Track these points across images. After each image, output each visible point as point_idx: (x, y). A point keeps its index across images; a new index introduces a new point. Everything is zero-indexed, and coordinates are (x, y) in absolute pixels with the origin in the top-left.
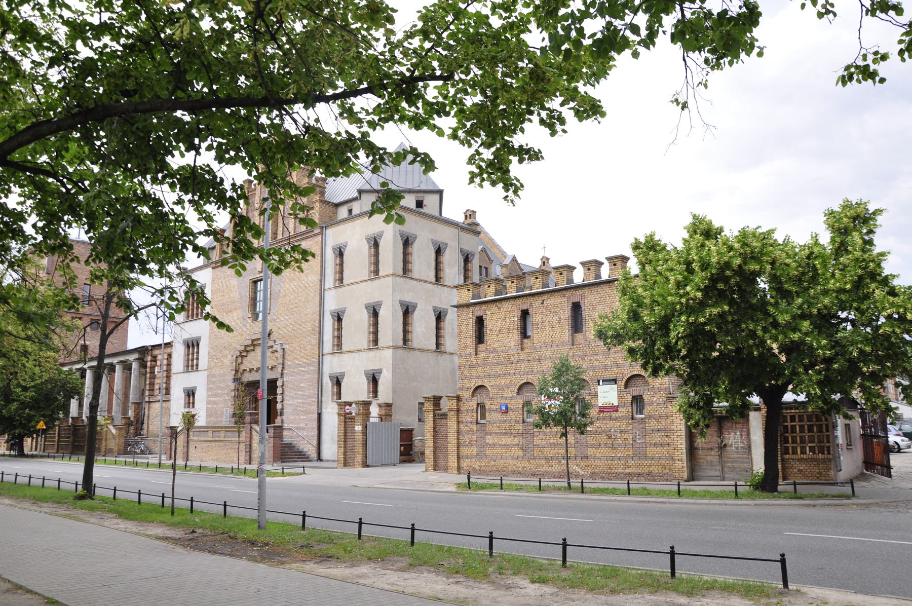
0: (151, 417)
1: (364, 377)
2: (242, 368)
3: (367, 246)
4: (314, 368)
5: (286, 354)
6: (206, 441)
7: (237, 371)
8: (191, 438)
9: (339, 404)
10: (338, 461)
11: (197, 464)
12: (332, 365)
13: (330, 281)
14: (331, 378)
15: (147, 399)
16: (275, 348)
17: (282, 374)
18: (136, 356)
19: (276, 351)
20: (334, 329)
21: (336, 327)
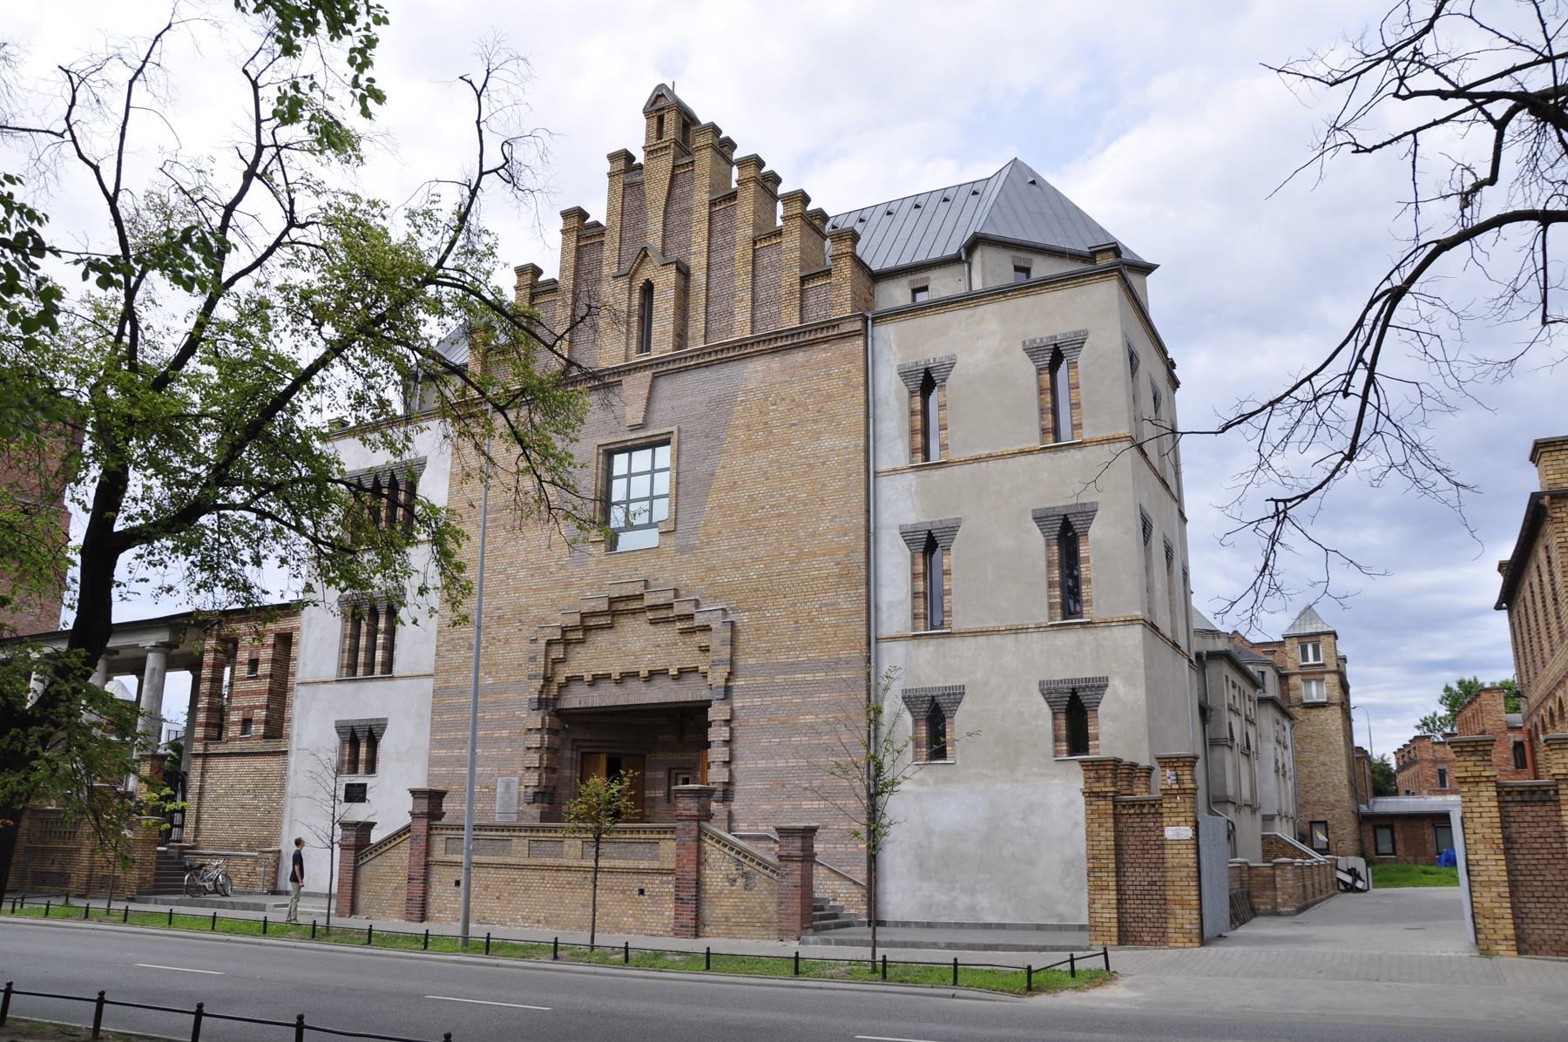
0: (208, 797)
1: (1041, 699)
2: (563, 673)
3: (1032, 369)
4: (855, 673)
5: (742, 637)
6: (507, 866)
7: (548, 680)
8: (438, 853)
9: (1088, 766)
10: (1090, 928)
11: (618, 940)
12: (911, 665)
13: (894, 447)
14: (910, 700)
15: (198, 748)
16: (699, 620)
17: (728, 691)
18: (164, 637)
19: (706, 629)
20: (914, 576)
21: (920, 568)
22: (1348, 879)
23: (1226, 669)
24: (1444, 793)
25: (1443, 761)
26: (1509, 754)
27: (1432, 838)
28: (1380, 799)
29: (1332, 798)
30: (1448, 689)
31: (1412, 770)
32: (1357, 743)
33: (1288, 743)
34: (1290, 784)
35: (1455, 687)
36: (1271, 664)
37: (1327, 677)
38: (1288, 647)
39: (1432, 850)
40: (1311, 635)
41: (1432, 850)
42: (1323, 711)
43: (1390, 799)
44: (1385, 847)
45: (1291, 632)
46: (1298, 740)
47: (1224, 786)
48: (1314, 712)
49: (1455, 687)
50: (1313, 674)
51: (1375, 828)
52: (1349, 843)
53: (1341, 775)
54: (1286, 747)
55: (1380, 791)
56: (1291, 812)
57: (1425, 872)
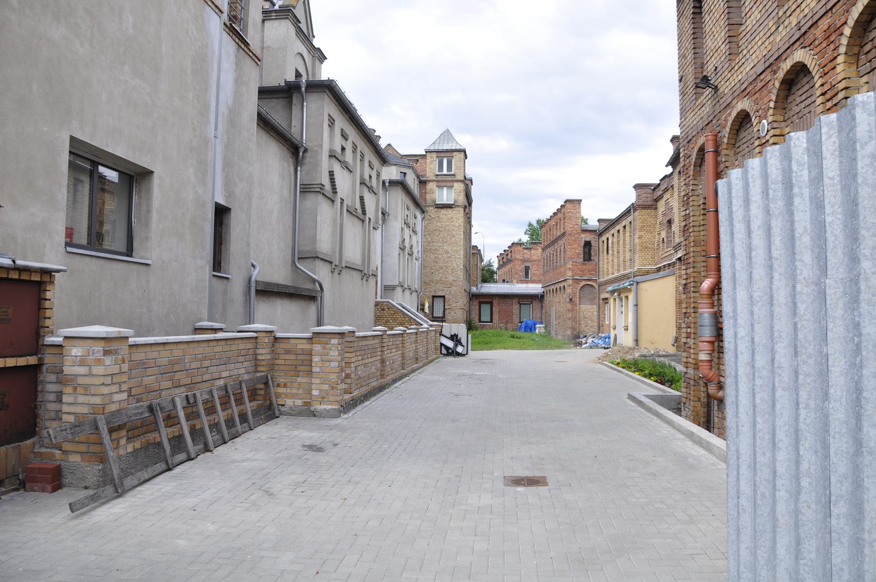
22: (450, 344)
23: (329, 108)
24: (527, 282)
25: (528, 261)
26: (580, 250)
27: (517, 312)
28: (485, 285)
29: (451, 278)
30: (530, 225)
31: (508, 267)
32: (473, 243)
33: (419, 229)
34: (417, 264)
35: (535, 224)
36: (412, 168)
37: (455, 184)
38: (429, 160)
39: (516, 319)
40: (447, 151)
41: (516, 319)
42: (450, 211)
43: (492, 285)
44: (486, 317)
45: (432, 148)
46: (427, 232)
47: (314, 240)
48: (444, 211)
49: (535, 224)
50: (445, 181)
51: (480, 303)
52: (460, 314)
53: (458, 262)
54: (415, 232)
55: (485, 280)
56: (416, 285)
57: (513, 337)
